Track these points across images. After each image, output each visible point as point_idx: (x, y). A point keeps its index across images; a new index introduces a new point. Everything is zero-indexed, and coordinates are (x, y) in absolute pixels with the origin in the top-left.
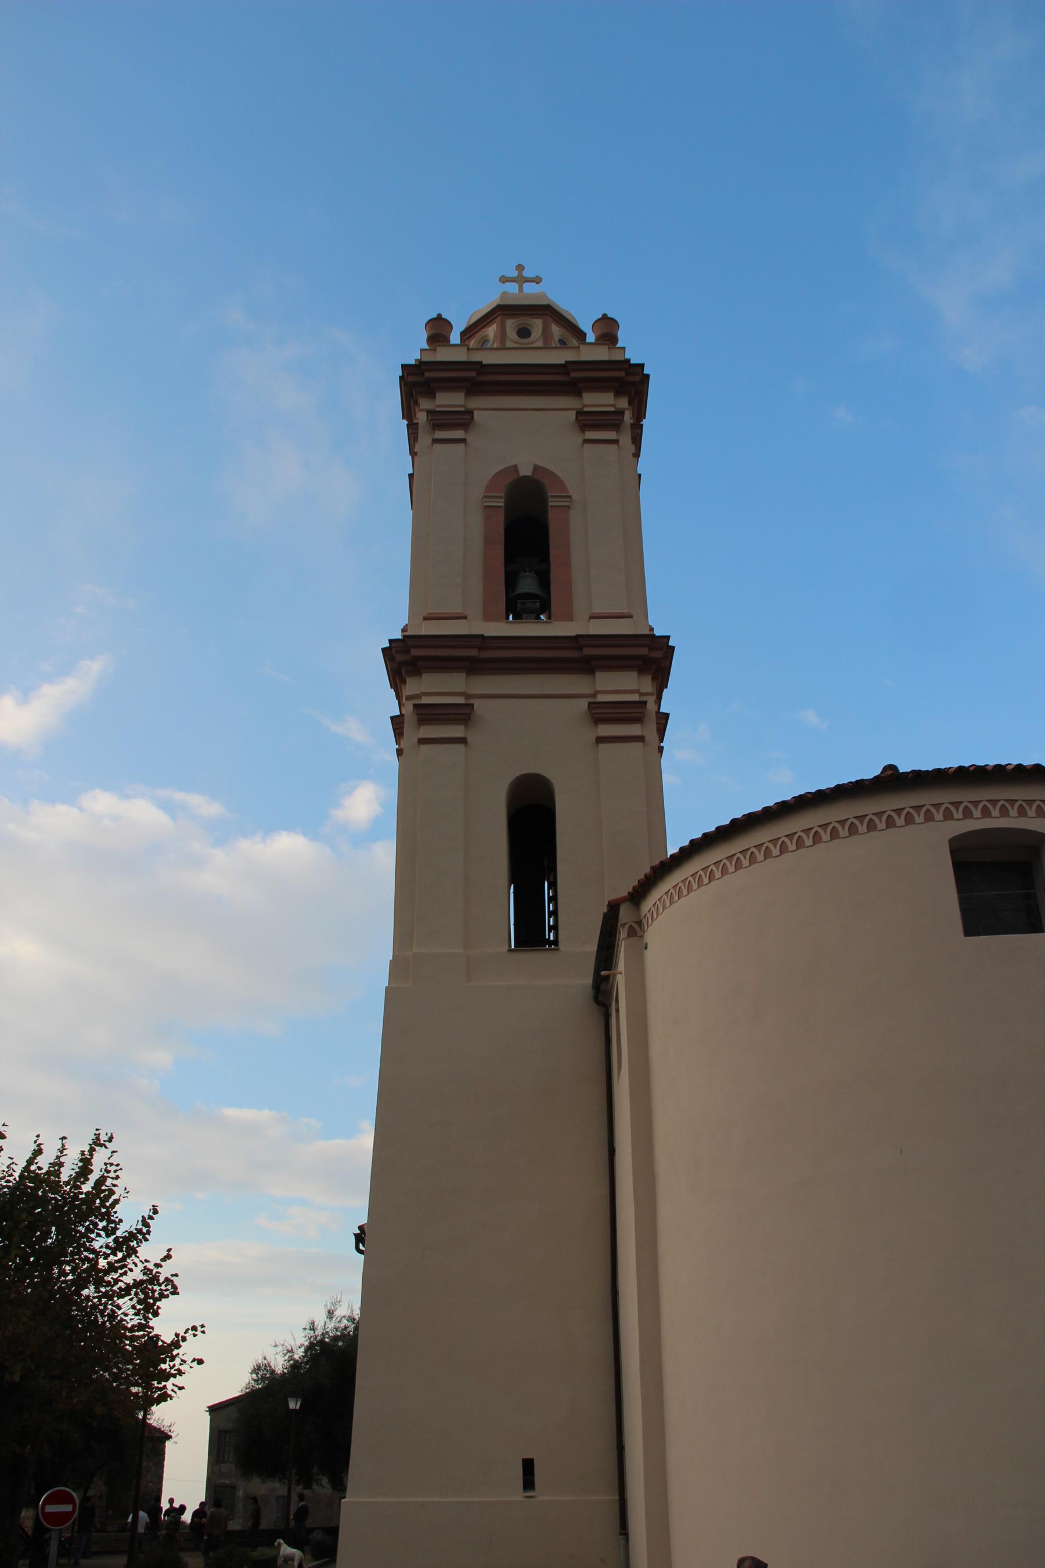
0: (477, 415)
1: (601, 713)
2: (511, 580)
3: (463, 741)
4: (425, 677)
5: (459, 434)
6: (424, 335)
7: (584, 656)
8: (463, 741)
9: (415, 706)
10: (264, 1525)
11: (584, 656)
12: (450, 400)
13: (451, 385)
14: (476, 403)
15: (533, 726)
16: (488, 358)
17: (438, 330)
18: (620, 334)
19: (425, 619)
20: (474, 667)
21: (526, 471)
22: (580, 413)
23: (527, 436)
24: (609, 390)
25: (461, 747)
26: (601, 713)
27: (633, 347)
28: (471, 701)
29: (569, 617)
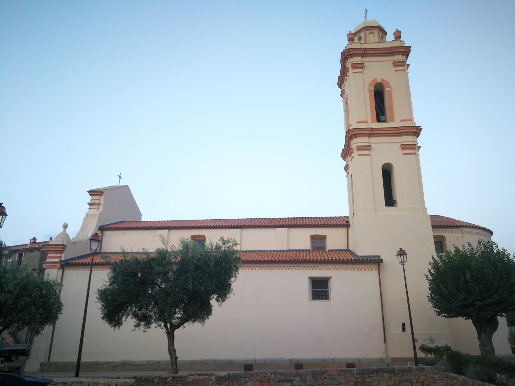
0: (365, 64)
1: (404, 147)
2: (383, 121)
3: (369, 155)
4: (358, 138)
5: (360, 70)
6: (347, 39)
7: (399, 132)
8: (369, 155)
9: (357, 146)
10: (91, 257)
11: (399, 132)
12: (357, 60)
13: (356, 55)
14: (365, 59)
15: (385, 150)
16: (367, 46)
17: (465, 319)
18: (402, 35)
19: (357, 122)
20: (370, 135)
21: (379, 81)
22: (394, 63)
23: (378, 70)
24: (399, 53)
25: (369, 156)
26: (404, 147)
27: (407, 40)
28: (370, 145)
29: (393, 120)
